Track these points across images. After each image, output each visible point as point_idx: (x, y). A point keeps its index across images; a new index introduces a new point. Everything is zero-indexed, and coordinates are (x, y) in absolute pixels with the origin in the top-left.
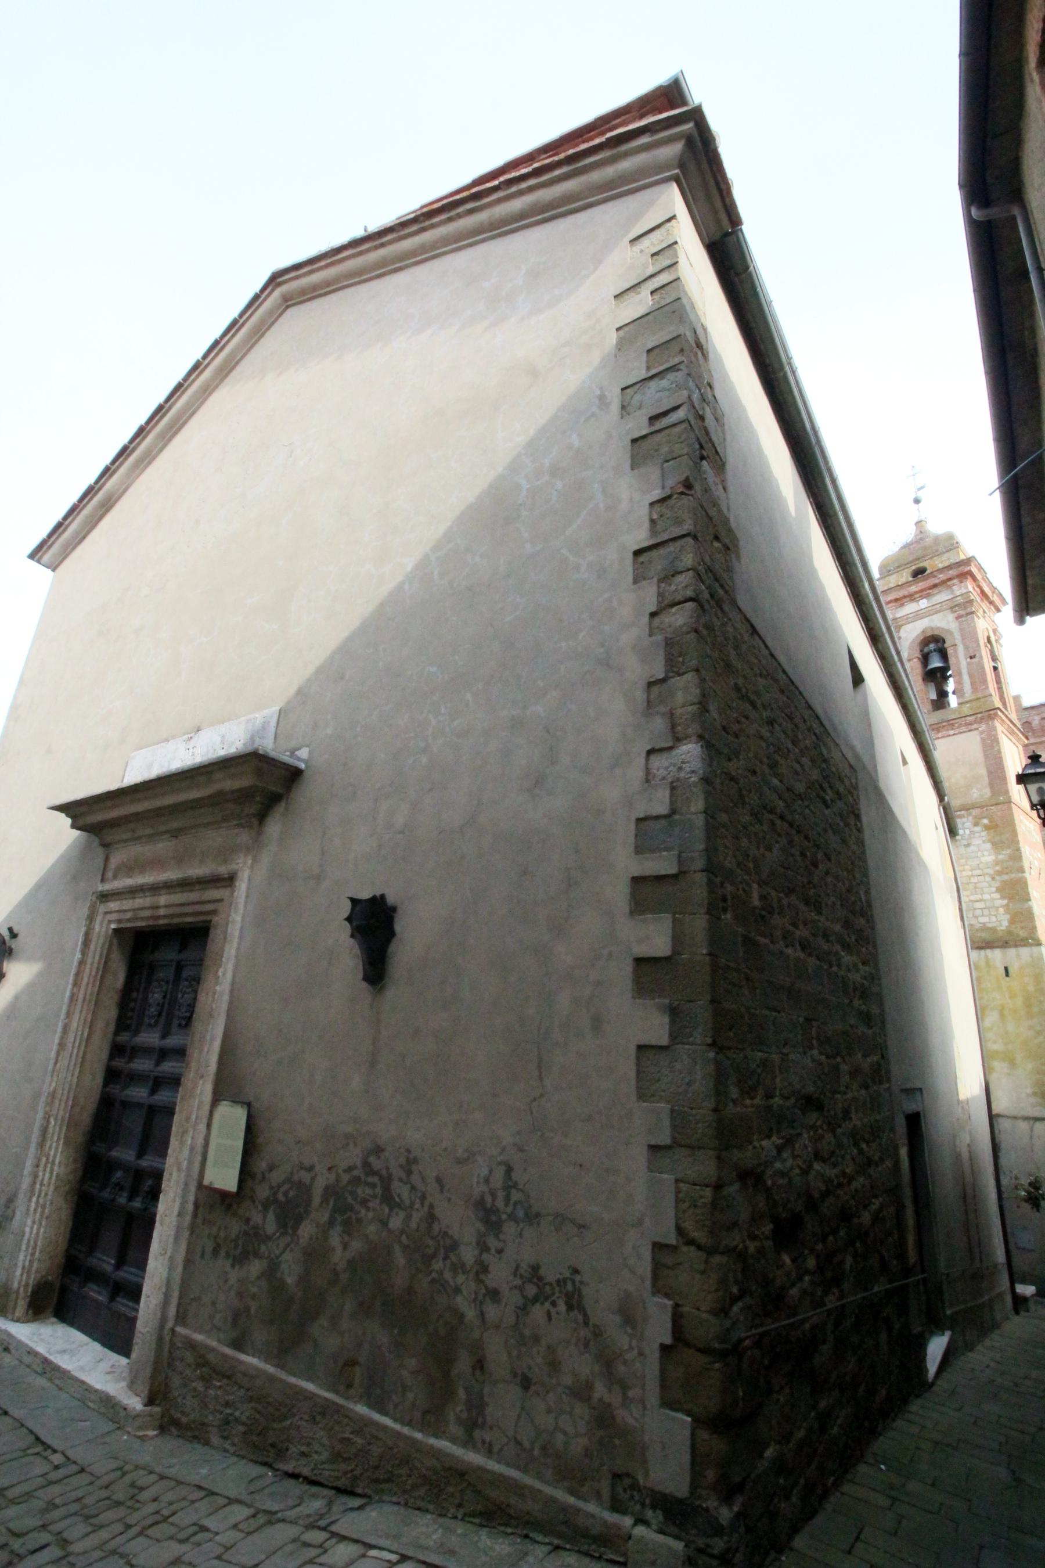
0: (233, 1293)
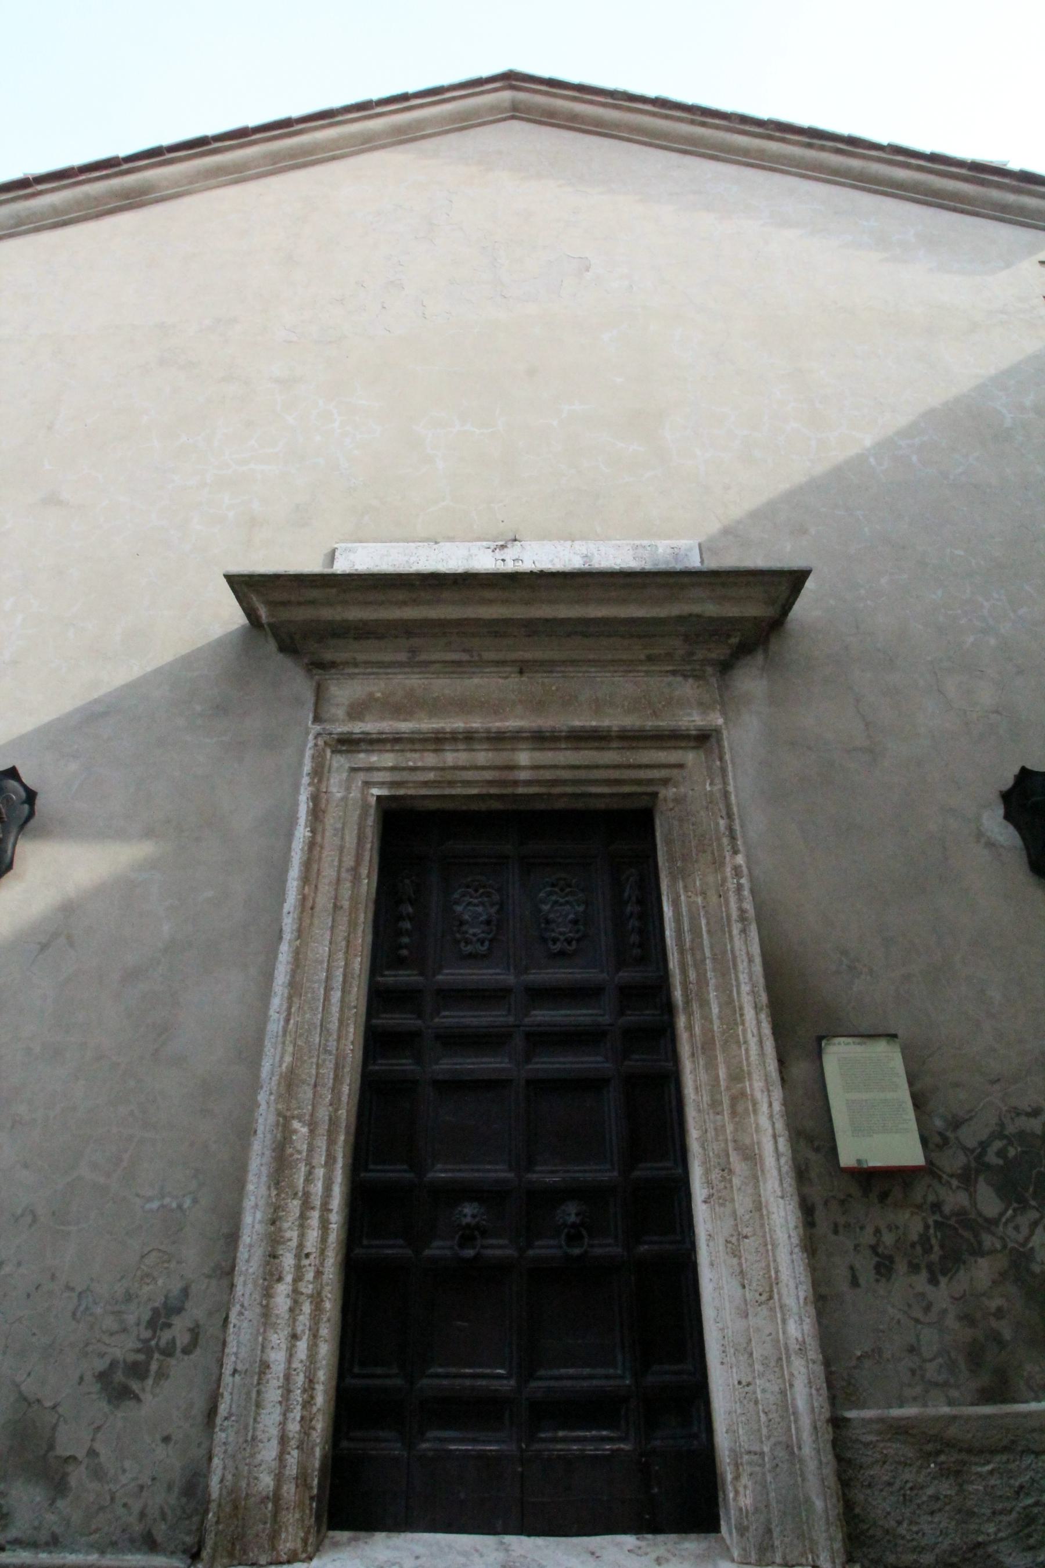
0: (951, 1322)
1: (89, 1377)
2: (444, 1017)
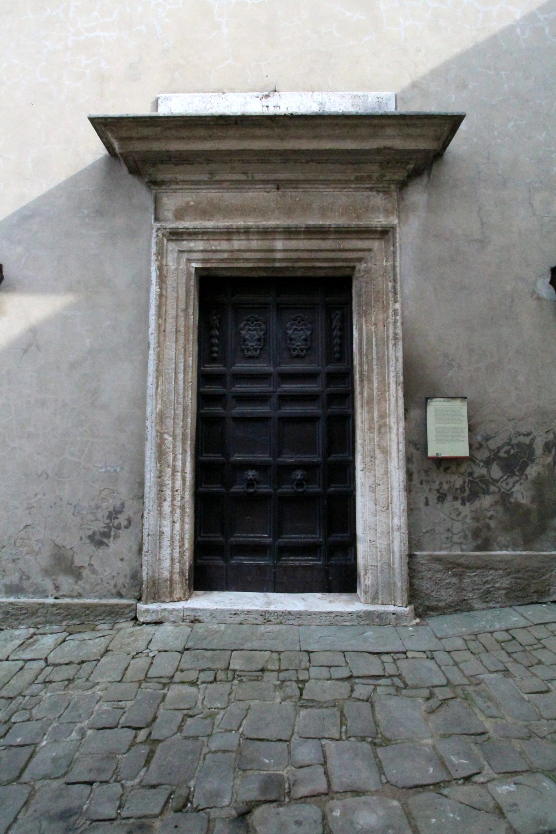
0: (468, 520)
1: (84, 537)
2: (237, 387)
